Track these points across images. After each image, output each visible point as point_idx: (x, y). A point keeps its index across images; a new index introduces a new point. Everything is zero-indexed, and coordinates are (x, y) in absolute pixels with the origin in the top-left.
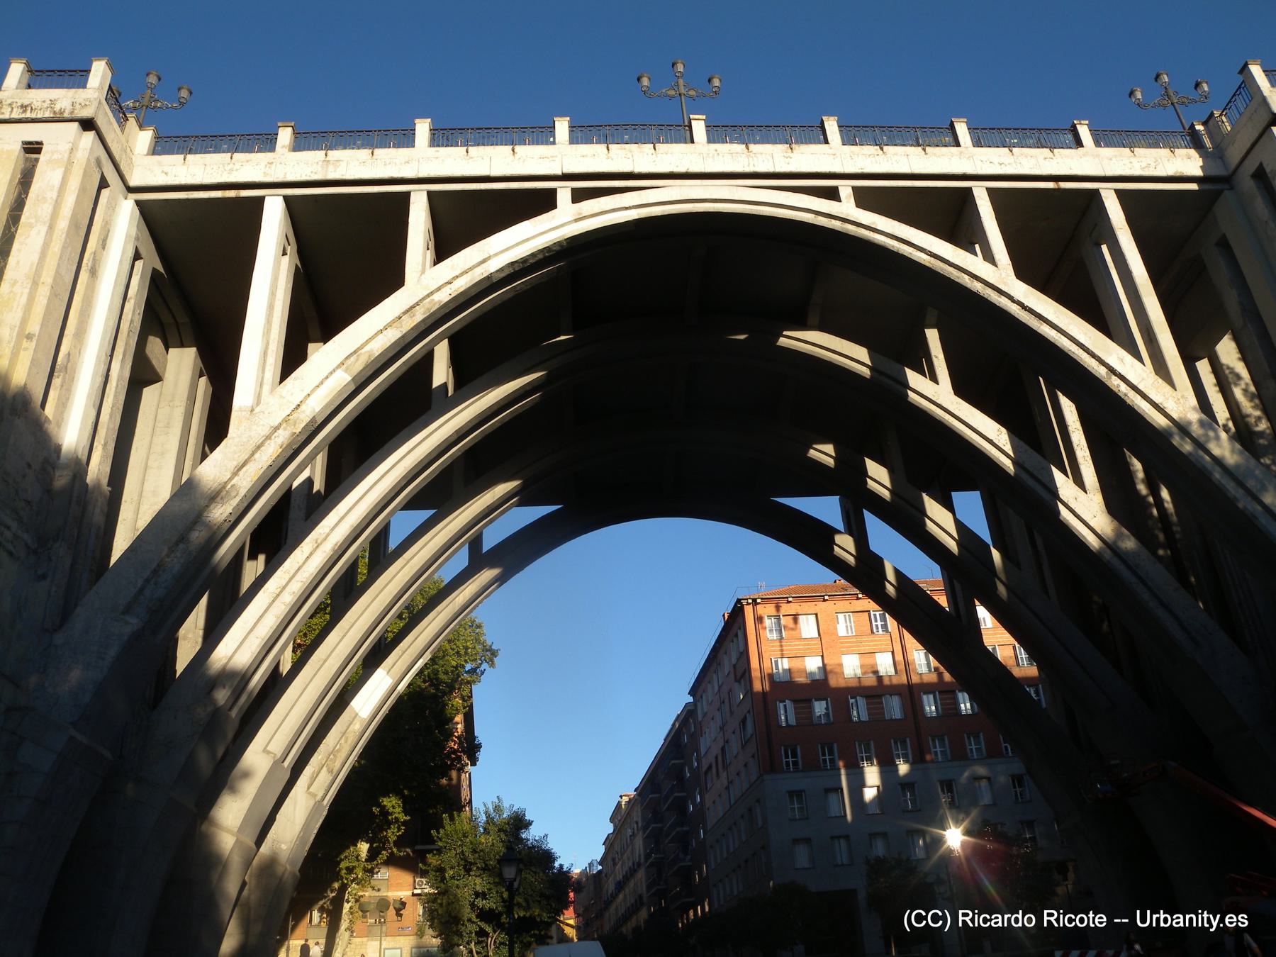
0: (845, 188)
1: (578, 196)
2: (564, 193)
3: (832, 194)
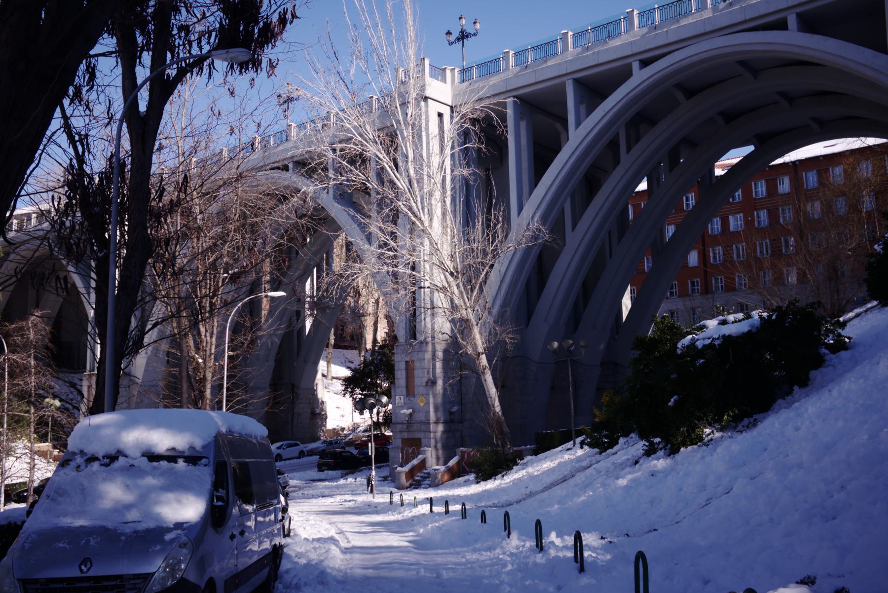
1: (645, 63)
2: (636, 66)
3: (781, 25)
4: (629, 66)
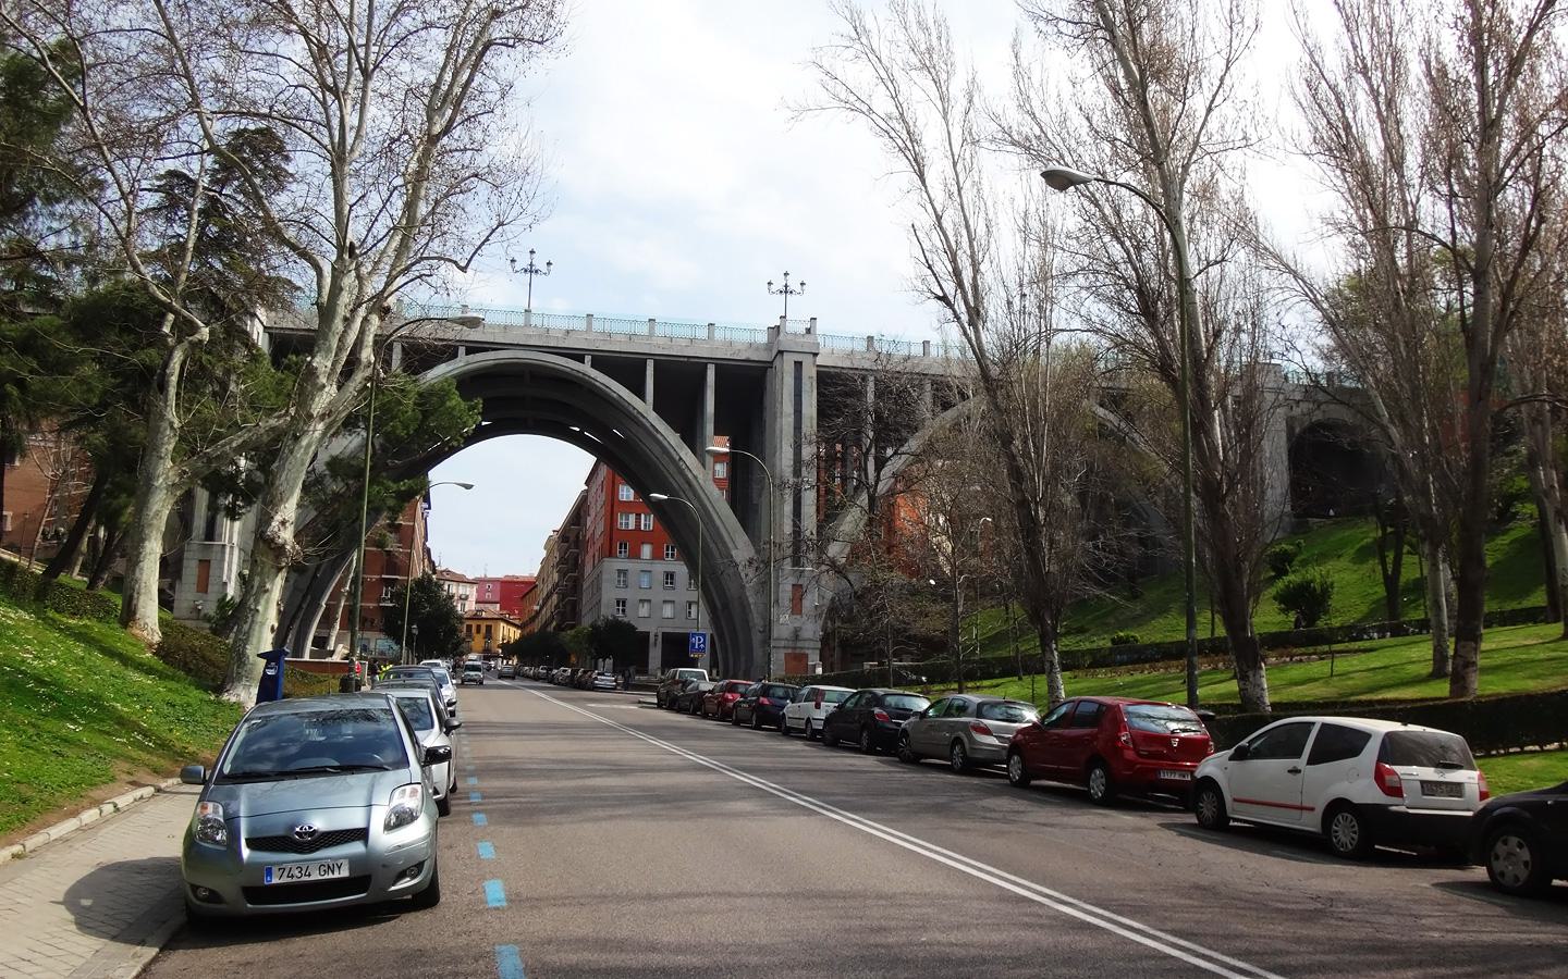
0: (588, 359)
1: (469, 351)
2: (462, 350)
3: (580, 359)
4: (456, 348)
